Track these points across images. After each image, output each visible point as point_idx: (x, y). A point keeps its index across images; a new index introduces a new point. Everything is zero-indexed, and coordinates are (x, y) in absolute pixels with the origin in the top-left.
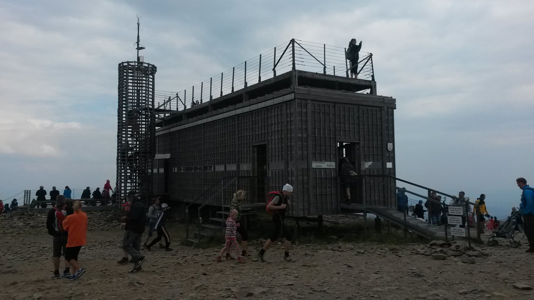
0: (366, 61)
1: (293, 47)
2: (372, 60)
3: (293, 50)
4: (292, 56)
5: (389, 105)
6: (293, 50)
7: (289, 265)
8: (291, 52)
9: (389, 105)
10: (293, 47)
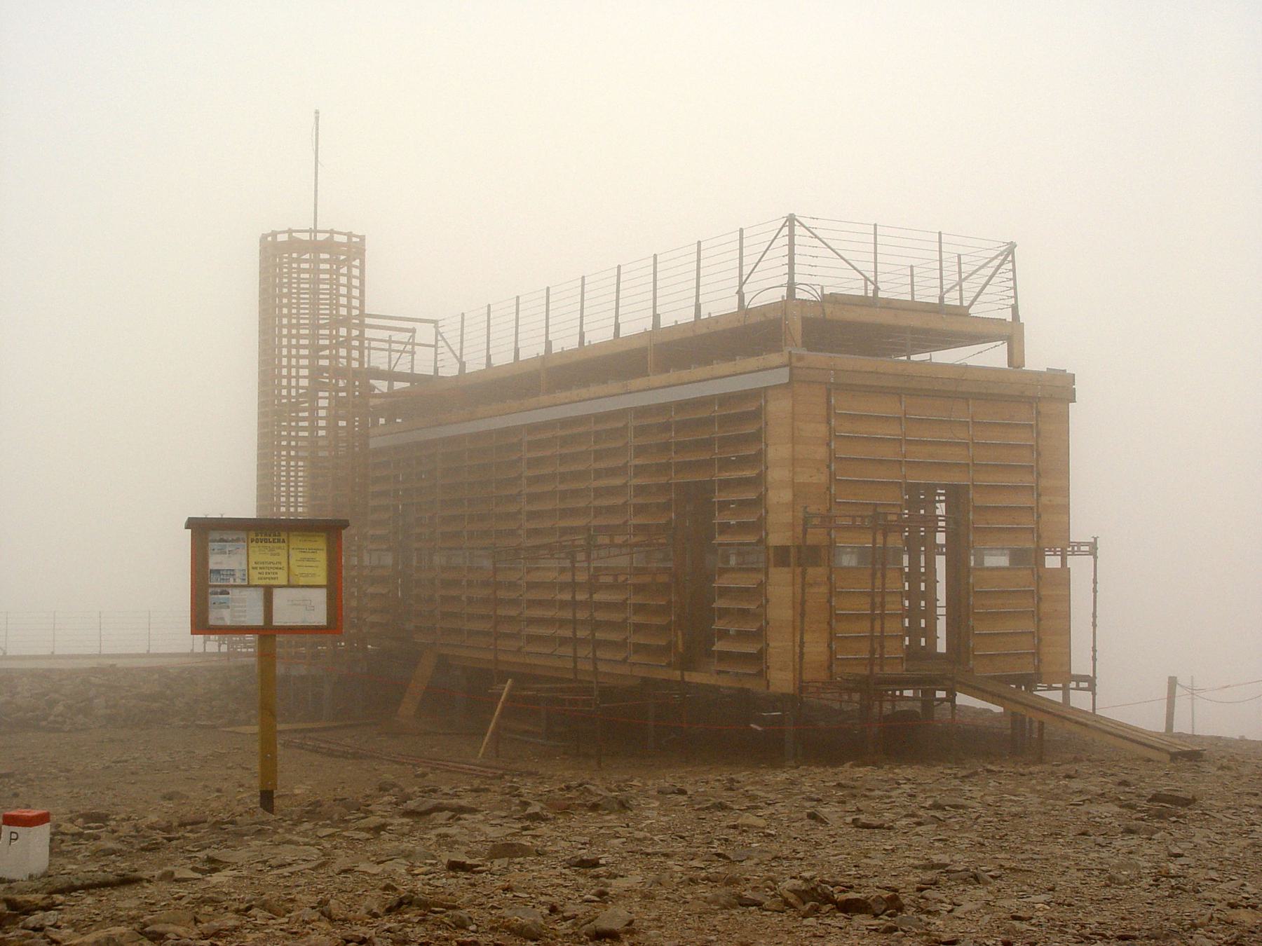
0: (988, 271)
1: (791, 236)
2: (1013, 261)
3: (791, 245)
4: (786, 260)
5: (1053, 394)
6: (791, 245)
7: (894, 883)
8: (786, 250)
9: (1053, 394)
10: (791, 236)
